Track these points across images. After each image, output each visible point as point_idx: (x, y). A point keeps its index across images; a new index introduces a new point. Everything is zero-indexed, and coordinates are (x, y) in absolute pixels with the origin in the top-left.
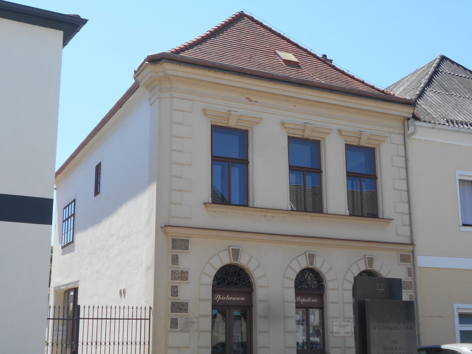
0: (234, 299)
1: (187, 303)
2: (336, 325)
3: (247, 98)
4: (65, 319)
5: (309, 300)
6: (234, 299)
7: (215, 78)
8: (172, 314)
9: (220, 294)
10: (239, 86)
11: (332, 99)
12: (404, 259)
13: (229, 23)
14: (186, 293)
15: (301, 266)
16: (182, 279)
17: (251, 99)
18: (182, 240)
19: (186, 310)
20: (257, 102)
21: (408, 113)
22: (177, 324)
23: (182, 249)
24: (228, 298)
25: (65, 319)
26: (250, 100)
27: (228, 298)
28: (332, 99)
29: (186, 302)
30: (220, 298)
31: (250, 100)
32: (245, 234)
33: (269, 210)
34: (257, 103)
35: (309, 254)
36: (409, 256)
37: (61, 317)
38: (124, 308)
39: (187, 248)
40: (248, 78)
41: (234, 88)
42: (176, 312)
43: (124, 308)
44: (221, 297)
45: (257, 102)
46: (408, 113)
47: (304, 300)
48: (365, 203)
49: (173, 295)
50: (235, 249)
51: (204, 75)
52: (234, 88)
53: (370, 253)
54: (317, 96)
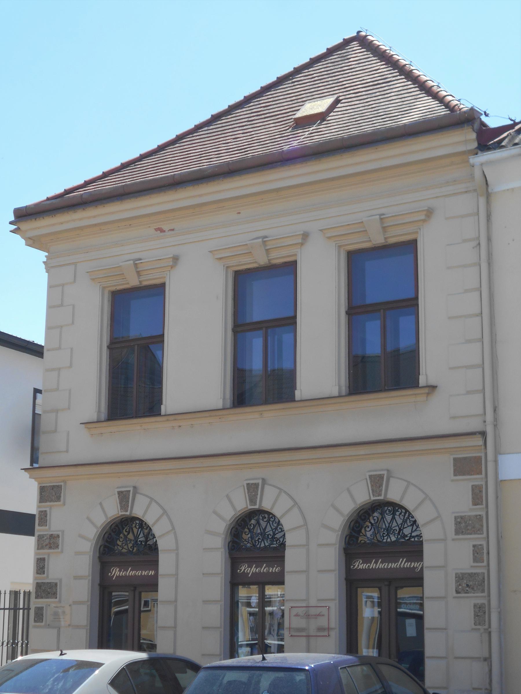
0: (139, 573)
1: (56, 584)
2: (297, 615)
3: (156, 230)
4: (7, 609)
5: (264, 569)
6: (139, 573)
7: (89, 218)
8: (37, 600)
9: (118, 566)
10: (223, 197)
11: (276, 180)
12: (465, 466)
13: (384, 57)
14: (58, 568)
15: (402, 497)
16: (50, 548)
17: (165, 227)
18: (53, 487)
19: (38, 596)
20: (173, 230)
21: (466, 141)
22: (42, 615)
23: (51, 501)
24: (130, 573)
25: (7, 609)
26: (162, 231)
27: (130, 573)
28: (276, 180)
29: (55, 581)
30: (117, 573)
31: (162, 231)
32: (202, 460)
33: (198, 415)
34: (172, 232)
35: (130, 491)
36: (480, 458)
37: (7, 606)
38: (5, 594)
39: (58, 499)
40: (133, 200)
41: (219, 204)
42: (42, 598)
43: (5, 594)
44: (120, 571)
45: (173, 230)
46: (466, 141)
47: (253, 569)
48: (383, 366)
49: (39, 572)
50: (122, 492)
51: (74, 220)
52: (129, 222)
53: (377, 465)
54: (173, 201)
